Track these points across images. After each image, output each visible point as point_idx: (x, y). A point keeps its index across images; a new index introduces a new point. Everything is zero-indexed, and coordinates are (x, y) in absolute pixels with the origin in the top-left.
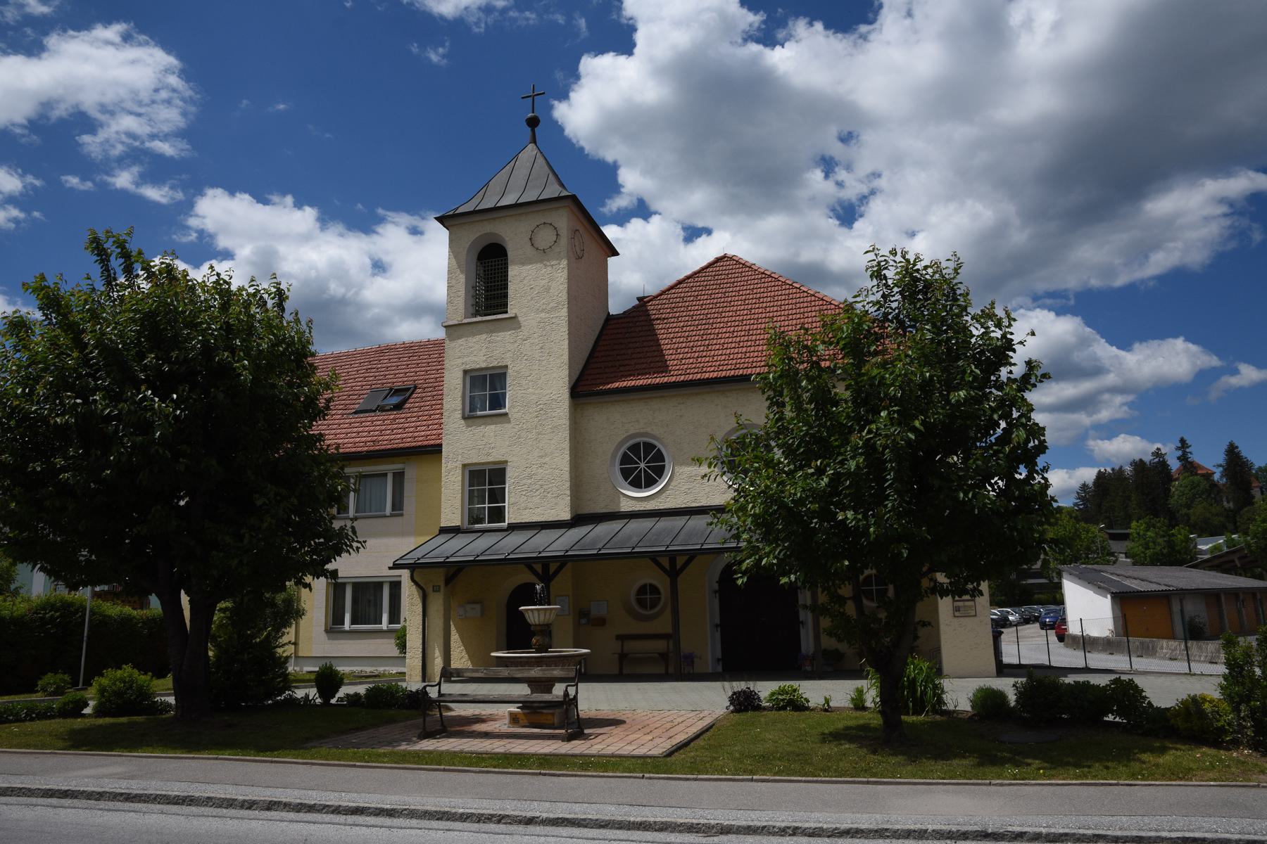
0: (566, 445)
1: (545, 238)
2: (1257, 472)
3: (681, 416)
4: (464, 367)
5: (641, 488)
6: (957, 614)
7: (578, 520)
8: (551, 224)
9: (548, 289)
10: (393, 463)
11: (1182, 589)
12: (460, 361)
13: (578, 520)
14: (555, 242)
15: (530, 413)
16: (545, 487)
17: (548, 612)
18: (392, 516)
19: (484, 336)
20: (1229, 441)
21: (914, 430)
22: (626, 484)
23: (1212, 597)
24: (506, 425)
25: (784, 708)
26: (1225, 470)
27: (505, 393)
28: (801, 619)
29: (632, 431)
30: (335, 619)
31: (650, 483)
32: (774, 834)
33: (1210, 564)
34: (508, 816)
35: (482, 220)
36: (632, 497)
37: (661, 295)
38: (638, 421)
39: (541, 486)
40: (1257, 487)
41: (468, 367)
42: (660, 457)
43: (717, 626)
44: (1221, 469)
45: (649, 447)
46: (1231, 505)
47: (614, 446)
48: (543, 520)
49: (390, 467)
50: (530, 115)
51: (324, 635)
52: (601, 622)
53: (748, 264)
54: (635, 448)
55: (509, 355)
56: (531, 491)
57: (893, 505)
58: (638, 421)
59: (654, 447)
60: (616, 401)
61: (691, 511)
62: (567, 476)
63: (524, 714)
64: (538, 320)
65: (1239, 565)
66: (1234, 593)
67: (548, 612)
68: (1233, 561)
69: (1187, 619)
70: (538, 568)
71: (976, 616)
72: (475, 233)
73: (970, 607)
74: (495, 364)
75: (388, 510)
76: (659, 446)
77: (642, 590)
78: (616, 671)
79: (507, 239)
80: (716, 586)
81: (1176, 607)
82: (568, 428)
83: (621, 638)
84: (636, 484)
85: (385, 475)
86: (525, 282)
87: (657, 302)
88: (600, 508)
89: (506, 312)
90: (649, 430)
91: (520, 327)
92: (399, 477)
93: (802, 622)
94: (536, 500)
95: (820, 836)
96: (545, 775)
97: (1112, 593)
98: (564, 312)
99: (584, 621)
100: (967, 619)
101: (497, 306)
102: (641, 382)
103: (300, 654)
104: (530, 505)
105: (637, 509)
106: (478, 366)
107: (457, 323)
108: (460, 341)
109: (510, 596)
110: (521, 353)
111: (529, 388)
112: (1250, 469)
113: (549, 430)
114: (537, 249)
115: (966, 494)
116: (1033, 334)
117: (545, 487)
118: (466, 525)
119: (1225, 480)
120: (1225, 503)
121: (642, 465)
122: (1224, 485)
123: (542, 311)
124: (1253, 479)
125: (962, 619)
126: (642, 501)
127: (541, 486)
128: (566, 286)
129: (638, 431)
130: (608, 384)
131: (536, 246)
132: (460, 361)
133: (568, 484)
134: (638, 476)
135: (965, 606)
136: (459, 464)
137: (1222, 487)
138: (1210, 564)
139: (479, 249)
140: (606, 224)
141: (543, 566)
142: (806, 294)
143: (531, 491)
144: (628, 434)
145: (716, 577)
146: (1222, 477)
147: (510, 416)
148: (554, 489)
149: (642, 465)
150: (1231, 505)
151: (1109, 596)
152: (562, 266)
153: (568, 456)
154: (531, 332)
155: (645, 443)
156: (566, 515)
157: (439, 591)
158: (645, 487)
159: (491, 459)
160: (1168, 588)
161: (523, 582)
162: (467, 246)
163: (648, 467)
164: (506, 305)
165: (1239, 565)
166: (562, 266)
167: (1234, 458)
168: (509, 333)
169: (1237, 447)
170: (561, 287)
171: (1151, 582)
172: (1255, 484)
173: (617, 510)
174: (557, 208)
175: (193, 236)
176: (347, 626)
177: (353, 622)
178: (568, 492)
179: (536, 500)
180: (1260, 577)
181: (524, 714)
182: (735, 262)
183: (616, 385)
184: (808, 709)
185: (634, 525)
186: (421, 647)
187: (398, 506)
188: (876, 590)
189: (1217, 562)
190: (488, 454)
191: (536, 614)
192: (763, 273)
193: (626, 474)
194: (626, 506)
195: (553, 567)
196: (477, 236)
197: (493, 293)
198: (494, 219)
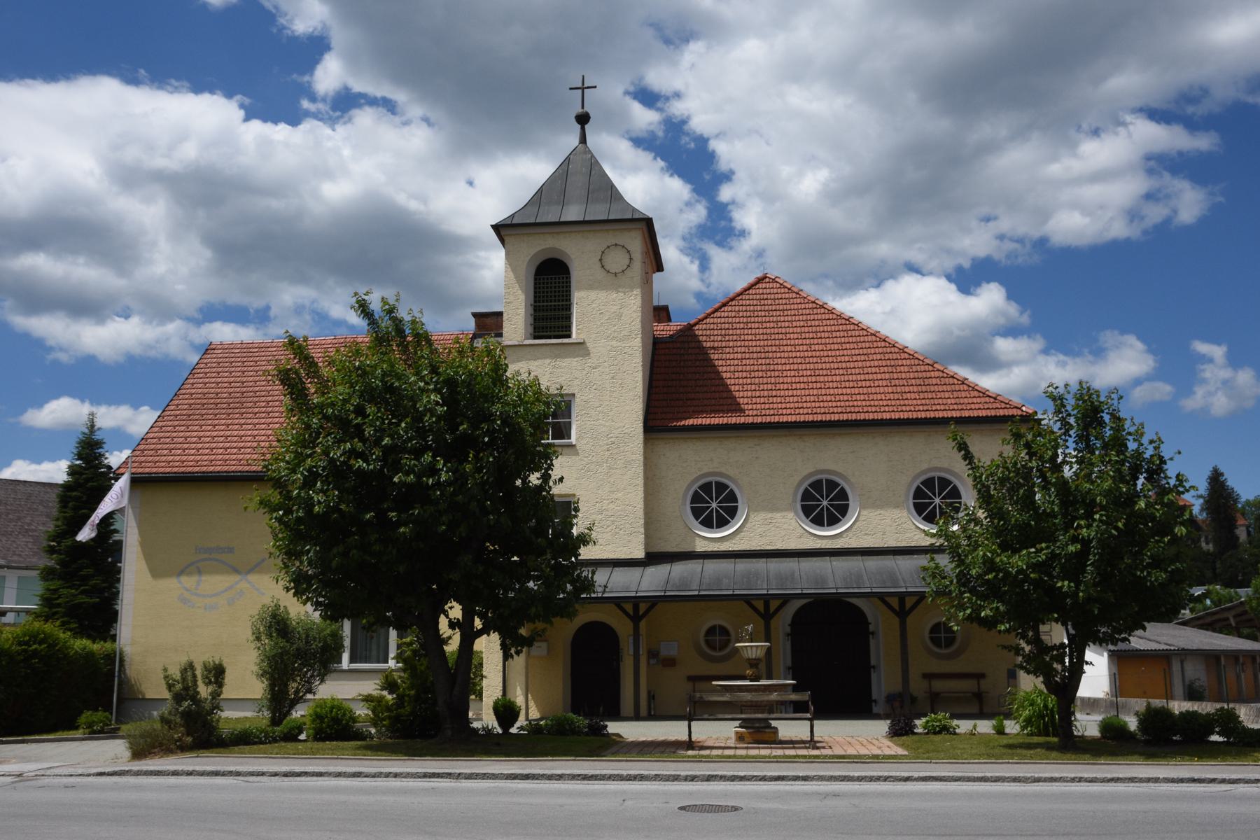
0: (640, 481)
1: (617, 260)
2: (1243, 507)
3: (757, 458)
5: (713, 528)
7: (653, 558)
8: (629, 252)
9: (620, 316)
11: (1183, 649)
13: (653, 558)
14: (629, 266)
15: (601, 446)
16: (617, 523)
17: (754, 649)
19: (548, 361)
20: (1214, 465)
21: (1117, 528)
23: (1212, 658)
24: (574, 457)
25: (940, 732)
26: (1207, 502)
27: (570, 423)
29: (705, 470)
31: (722, 523)
32: (1067, 781)
33: (1201, 622)
34: (891, 777)
36: (707, 538)
37: (706, 318)
38: (712, 460)
39: (613, 522)
40: (1243, 525)
43: (789, 668)
44: (1201, 501)
45: (721, 487)
46: (1211, 547)
47: (686, 485)
50: (580, 110)
52: (670, 663)
53: (795, 289)
55: (576, 382)
57: (414, 459)
58: (712, 460)
60: (688, 438)
61: (767, 554)
63: (750, 733)
64: (609, 348)
65: (1234, 624)
66: (1234, 656)
67: (760, 648)
68: (1227, 619)
69: (1187, 682)
70: (760, 605)
72: (535, 247)
76: (732, 486)
77: (711, 631)
78: (632, 714)
79: (573, 257)
80: (788, 630)
81: (1176, 667)
82: (642, 464)
83: (693, 679)
84: (707, 524)
86: (594, 306)
87: (704, 327)
90: (723, 470)
91: (589, 354)
95: (1095, 782)
96: (857, 762)
97: (1110, 651)
99: (653, 661)
105: (710, 550)
107: (517, 343)
111: (598, 420)
112: (1236, 501)
114: (603, 267)
115: (1142, 572)
116: (1180, 453)
117: (617, 523)
119: (1205, 514)
120: (1203, 544)
121: (714, 505)
122: (1204, 521)
123: (614, 339)
124: (1238, 515)
126: (715, 542)
127: (613, 522)
128: (640, 314)
129: (711, 470)
130: (681, 419)
131: (607, 268)
133: (642, 522)
137: (1200, 523)
138: (1201, 622)
139: (538, 263)
142: (865, 333)
144: (702, 473)
145: (789, 621)
146: (1202, 510)
147: (578, 447)
148: (627, 525)
149: (714, 505)
150: (1211, 547)
151: (1106, 654)
153: (642, 492)
154: (601, 360)
155: (717, 483)
156: (640, 554)
158: (717, 528)
160: (1168, 647)
161: (598, 620)
162: (528, 259)
163: (720, 507)
164: (569, 328)
165: (1234, 624)
167: (1218, 489)
169: (1222, 474)
170: (635, 315)
171: (1150, 640)
172: (1241, 521)
174: (630, 230)
177: (352, 660)
178: (642, 530)
180: (1255, 639)
181: (750, 733)
182: (778, 286)
183: (690, 422)
184: (955, 734)
185: (712, 566)
186: (501, 684)
189: (1209, 620)
191: (754, 649)
192: (814, 302)
193: (696, 513)
194: (700, 547)
196: (539, 248)
198: (558, 233)
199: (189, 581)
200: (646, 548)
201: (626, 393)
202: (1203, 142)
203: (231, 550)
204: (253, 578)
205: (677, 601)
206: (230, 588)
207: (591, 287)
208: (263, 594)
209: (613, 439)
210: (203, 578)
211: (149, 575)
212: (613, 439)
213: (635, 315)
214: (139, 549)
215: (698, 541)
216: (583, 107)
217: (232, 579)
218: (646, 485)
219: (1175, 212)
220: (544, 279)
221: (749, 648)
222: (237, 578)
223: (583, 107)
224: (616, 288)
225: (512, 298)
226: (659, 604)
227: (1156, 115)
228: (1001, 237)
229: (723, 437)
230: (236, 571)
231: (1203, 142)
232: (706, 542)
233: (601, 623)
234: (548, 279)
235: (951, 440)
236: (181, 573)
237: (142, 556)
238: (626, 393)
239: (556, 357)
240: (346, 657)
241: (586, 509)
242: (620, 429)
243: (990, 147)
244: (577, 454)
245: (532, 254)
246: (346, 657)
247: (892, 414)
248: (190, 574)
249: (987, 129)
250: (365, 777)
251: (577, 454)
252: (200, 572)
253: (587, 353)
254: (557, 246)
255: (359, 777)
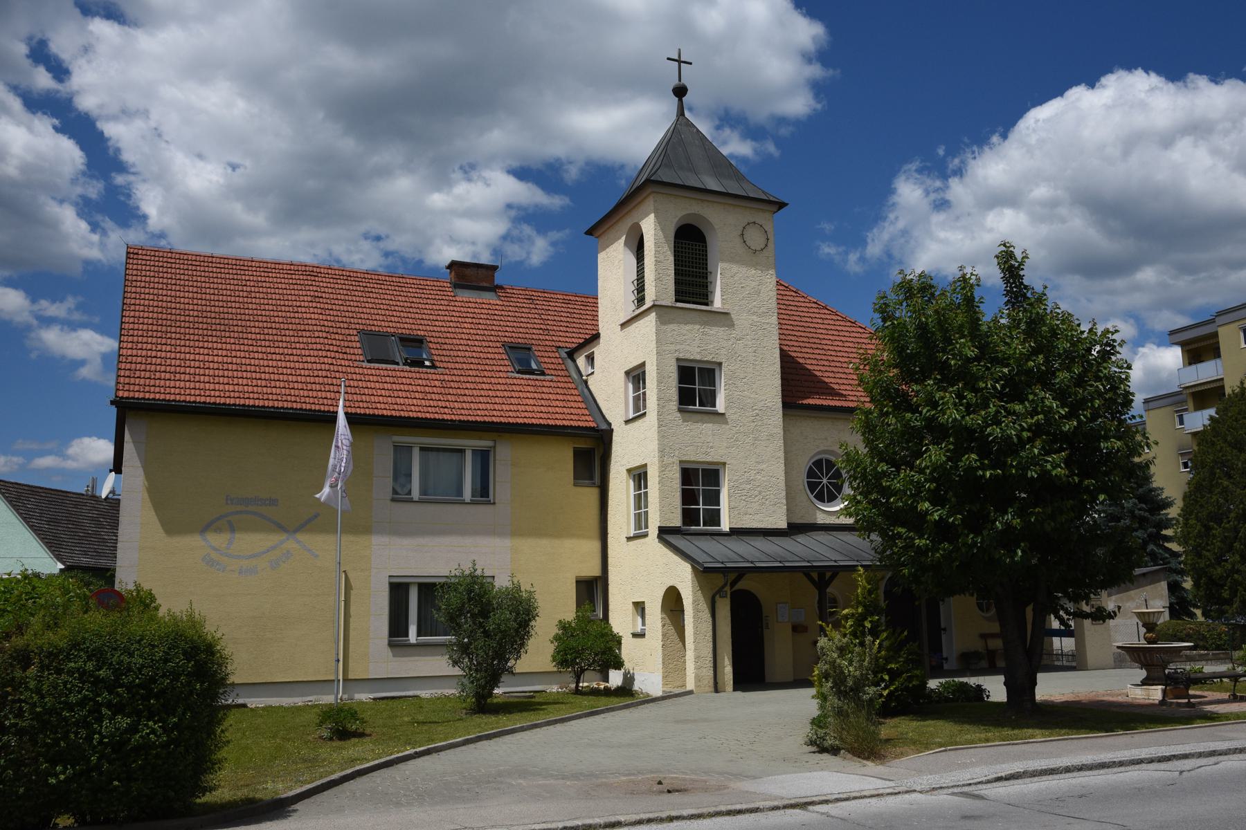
0: (781, 454)
4: (676, 354)
10: (480, 439)
12: (672, 347)
18: (472, 503)
19: (697, 327)
24: (724, 426)
28: (943, 626)
29: (822, 448)
30: (397, 627)
35: (746, 207)
38: (826, 439)
39: (760, 492)
41: (681, 356)
48: (762, 526)
49: (471, 443)
51: (387, 652)
55: (723, 351)
56: (750, 497)
62: (782, 485)
70: (815, 575)
74: (709, 358)
75: (467, 494)
85: (461, 451)
89: (707, 304)
91: (733, 325)
92: (484, 460)
93: (944, 629)
98: (774, 320)
101: (693, 294)
102: (825, 403)
103: (351, 677)
104: (750, 511)
105: (827, 522)
106: (692, 357)
108: (672, 326)
110: (736, 353)
111: (744, 391)
113: (765, 438)
129: (826, 448)
132: (672, 347)
133: (784, 493)
134: (822, 491)
136: (676, 460)
141: (818, 574)
143: (750, 497)
156: (783, 524)
157: (726, 597)
158: (828, 502)
159: (709, 459)
168: (723, 329)
176: (413, 636)
177: (419, 634)
178: (785, 501)
183: (811, 401)
187: (483, 491)
190: (707, 454)
195: (828, 575)
196: (684, 213)
197: (698, 280)
199: (217, 540)
200: (787, 519)
201: (767, 367)
202: (554, 202)
203: (273, 502)
204: (299, 536)
205: (776, 572)
206: (273, 548)
207: (732, 260)
208: (317, 556)
209: (757, 411)
210: (237, 535)
211: (161, 530)
212: (757, 411)
213: (771, 293)
214: (146, 495)
215: (818, 513)
216: (680, 80)
217: (273, 539)
218: (786, 459)
219: (528, 253)
220: (682, 243)
221: (1156, 614)
222: (284, 536)
223: (680, 80)
224: (755, 265)
225: (662, 258)
226: (840, 574)
227: (521, 173)
228: (387, 254)
229: (835, 418)
230: (281, 528)
231: (554, 202)
232: (824, 515)
233: (753, 594)
234: (682, 243)
235: (859, 433)
236: (205, 529)
237: (150, 505)
238: (767, 367)
239: (705, 324)
240: (413, 630)
241: (736, 478)
242: (763, 402)
243: (384, 172)
244: (727, 423)
245: (679, 216)
246: (413, 630)
247: (276, 402)
248: (219, 530)
249: (388, 155)
250: (1220, 755)
251: (727, 423)
252: (232, 529)
253: (731, 325)
254: (701, 213)
255: (1214, 755)
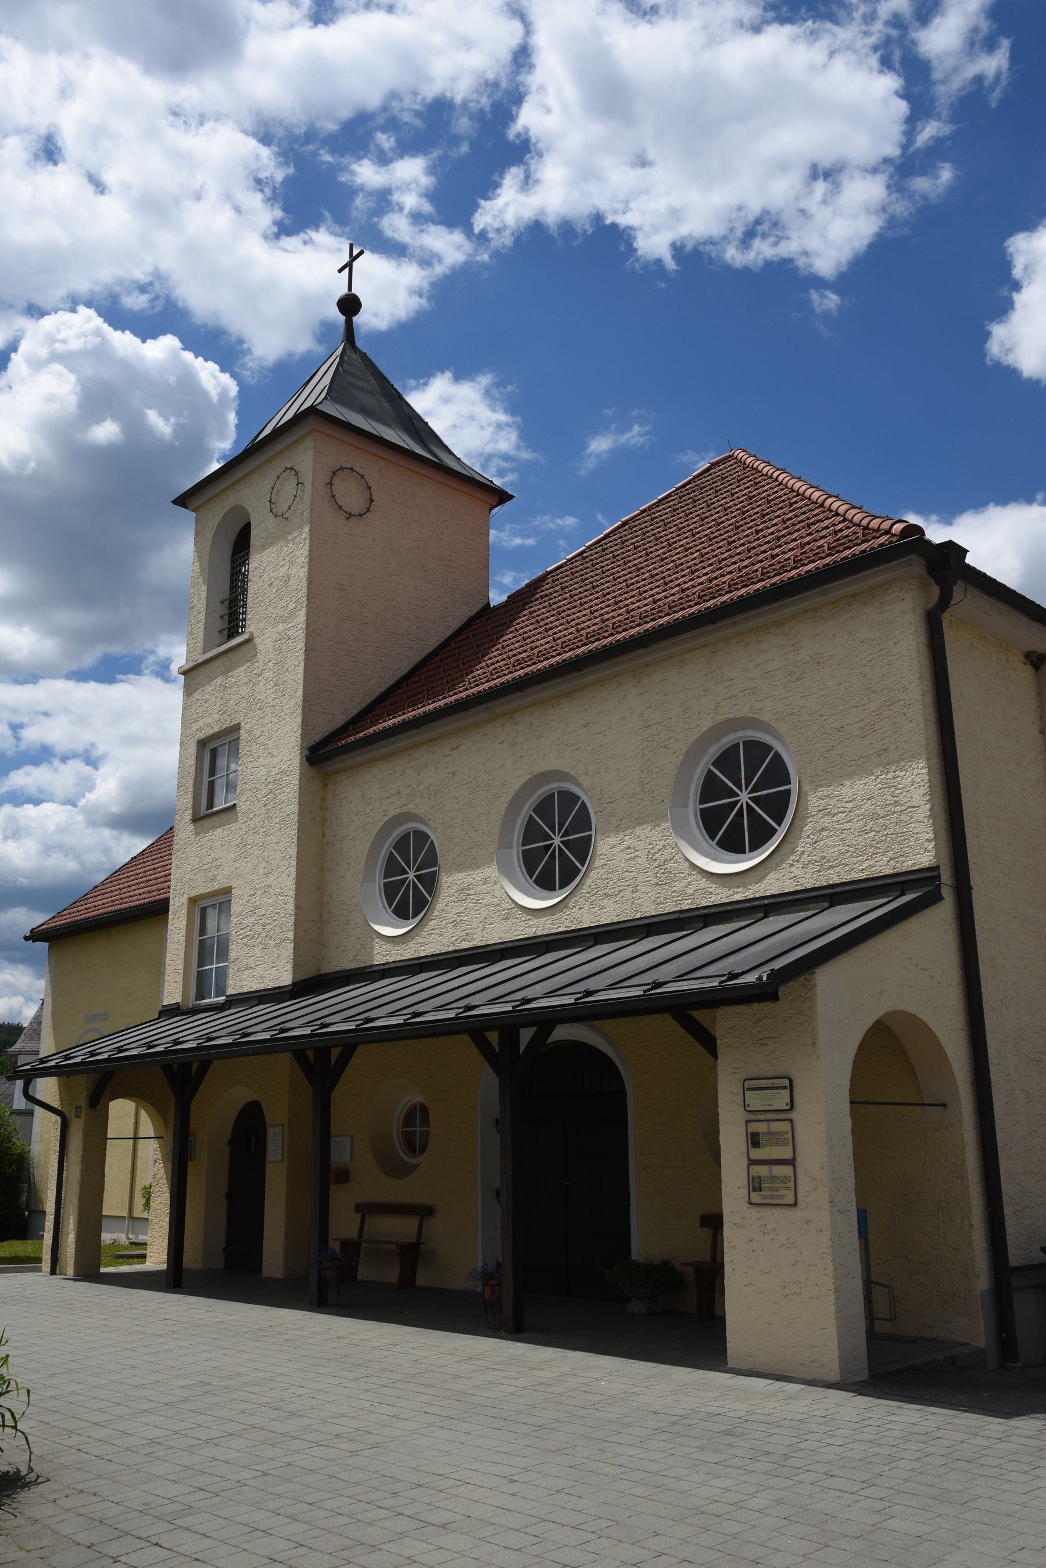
3: (454, 773)
5: (744, 852)
6: (756, 1197)
7: (303, 988)
22: (387, 913)
42: (778, 773)
45: (757, 750)
48: (262, 987)
54: (726, 760)
59: (767, 748)
71: (795, 1204)
72: (215, 515)
73: (784, 1180)
84: (732, 845)
88: (347, 962)
94: (257, 952)
100: (778, 1212)
105: (391, 960)
109: (244, 1107)
118: (192, 1002)
125: (766, 1212)
135: (773, 1178)
140: (424, 375)
152: (303, 537)
156: (286, 979)
158: (751, 851)
166: (303, 537)
173: (368, 964)
175: (494, 259)
179: (257, 952)
188: (416, 1127)
194: (382, 955)
